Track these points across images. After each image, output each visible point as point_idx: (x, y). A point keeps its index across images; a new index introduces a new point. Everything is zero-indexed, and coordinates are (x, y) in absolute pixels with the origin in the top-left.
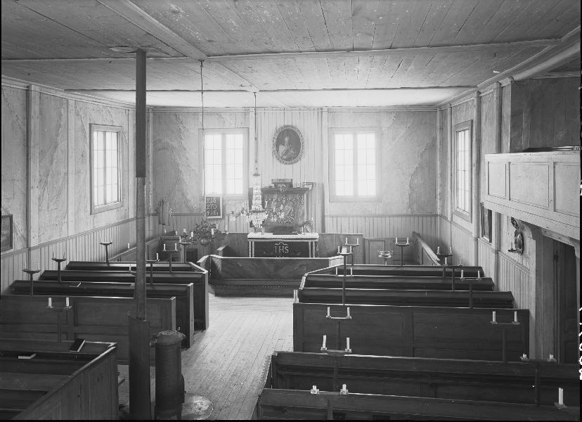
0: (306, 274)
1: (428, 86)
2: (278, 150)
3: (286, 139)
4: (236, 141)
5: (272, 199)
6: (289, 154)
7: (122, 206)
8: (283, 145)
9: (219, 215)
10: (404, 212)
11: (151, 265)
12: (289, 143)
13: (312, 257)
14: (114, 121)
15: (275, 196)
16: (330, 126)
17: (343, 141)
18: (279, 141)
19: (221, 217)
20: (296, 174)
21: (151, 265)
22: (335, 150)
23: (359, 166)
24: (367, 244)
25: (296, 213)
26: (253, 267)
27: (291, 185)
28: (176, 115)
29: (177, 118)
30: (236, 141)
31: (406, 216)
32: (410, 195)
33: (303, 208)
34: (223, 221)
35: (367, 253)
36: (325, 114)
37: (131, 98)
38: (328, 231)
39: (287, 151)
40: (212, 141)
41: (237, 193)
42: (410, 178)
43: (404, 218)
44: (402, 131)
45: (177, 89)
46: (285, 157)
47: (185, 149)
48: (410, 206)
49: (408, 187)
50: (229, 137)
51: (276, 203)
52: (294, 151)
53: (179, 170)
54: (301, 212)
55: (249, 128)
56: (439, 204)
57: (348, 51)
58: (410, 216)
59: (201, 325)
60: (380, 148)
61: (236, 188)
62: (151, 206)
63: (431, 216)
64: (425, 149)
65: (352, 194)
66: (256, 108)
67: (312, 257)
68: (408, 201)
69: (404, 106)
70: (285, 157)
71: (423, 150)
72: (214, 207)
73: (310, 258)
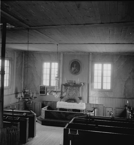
0: (74, 118)
1: (127, 43)
3: (75, 65)
4: (55, 65)
5: (67, 88)
7: (10, 88)
8: (73, 67)
9: (45, 94)
10: (122, 97)
14: (8, 56)
15: (69, 87)
18: (72, 66)
19: (45, 94)
20: (77, 79)
23: (49, 74)
24: (105, 108)
26: (57, 114)
27: (75, 84)
28: (33, 55)
29: (33, 56)
30: (55, 65)
32: (125, 90)
33: (79, 93)
35: (105, 112)
36: (91, 56)
38: (91, 102)
39: (75, 70)
40: (46, 65)
43: (122, 99)
44: (122, 63)
45: (36, 43)
46: (74, 72)
48: (124, 94)
49: (124, 87)
50: (53, 64)
51: (69, 90)
53: (33, 75)
55: (60, 60)
57: (84, 25)
58: (124, 98)
59: (32, 135)
61: (54, 83)
67: (82, 112)
68: (124, 92)
69: (124, 53)
70: (74, 72)
72: (43, 91)
73: (67, 112)
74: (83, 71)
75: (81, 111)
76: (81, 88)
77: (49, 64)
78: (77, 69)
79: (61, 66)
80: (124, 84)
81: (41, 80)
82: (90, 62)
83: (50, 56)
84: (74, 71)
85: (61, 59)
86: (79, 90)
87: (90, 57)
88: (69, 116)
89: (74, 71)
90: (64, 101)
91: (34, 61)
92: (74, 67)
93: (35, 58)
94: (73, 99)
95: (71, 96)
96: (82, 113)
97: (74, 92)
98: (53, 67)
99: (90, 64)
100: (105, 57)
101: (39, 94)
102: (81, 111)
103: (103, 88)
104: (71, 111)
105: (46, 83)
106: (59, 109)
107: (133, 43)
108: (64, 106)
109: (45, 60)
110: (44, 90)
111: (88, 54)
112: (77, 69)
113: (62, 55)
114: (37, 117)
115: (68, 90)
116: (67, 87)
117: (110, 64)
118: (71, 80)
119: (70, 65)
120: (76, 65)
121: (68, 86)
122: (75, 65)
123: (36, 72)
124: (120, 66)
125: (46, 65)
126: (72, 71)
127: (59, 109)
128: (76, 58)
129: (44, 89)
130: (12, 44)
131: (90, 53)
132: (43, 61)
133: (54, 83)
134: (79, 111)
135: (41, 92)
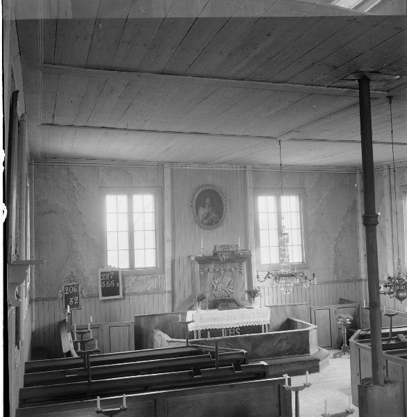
2: (197, 213)
4: (145, 203)
5: (208, 270)
6: (211, 217)
8: (204, 207)
10: (332, 278)
13: (197, 338)
15: (212, 267)
17: (265, 204)
18: (199, 203)
25: (235, 285)
30: (145, 203)
31: (334, 282)
34: (122, 302)
36: (249, 175)
37: (353, 155)
39: (208, 214)
43: (331, 285)
45: (113, 126)
46: (206, 221)
47: (80, 213)
48: (336, 272)
49: (333, 253)
50: (137, 198)
60: (304, 211)
61: (146, 258)
62: (140, 278)
64: (347, 212)
70: (206, 221)
71: (345, 212)
72: (112, 285)
74: (230, 216)
75: (263, 327)
77: (123, 199)
78: (214, 211)
79: (168, 204)
80: (333, 247)
81: (100, 249)
82: (250, 191)
83: (126, 174)
84: (206, 218)
85: (168, 182)
86: (240, 272)
87: (248, 180)
88: (263, 344)
89: (206, 218)
90: (205, 309)
92: (207, 205)
93: (76, 179)
94: (227, 298)
95: (220, 293)
96: (267, 333)
97: (227, 279)
98: (284, 208)
99: (250, 198)
100: (284, 179)
101: (101, 298)
102: (263, 327)
103: (136, 266)
104: (236, 334)
105: (116, 260)
106: (200, 334)
107: (357, 139)
108: (217, 323)
109: (113, 187)
110: (116, 284)
111: (92, 164)
112: (214, 211)
113: (167, 171)
114: (384, 350)
115: (210, 276)
117: (152, 193)
118: (224, 244)
119: (195, 201)
120: (210, 202)
121: (210, 263)
122: (208, 201)
123: (84, 225)
124: (321, 201)
127: (199, 332)
128: (209, 180)
129: (117, 280)
130: (325, 142)
131: (249, 167)
132: (104, 189)
133: (146, 258)
134: (257, 329)
135: (107, 292)
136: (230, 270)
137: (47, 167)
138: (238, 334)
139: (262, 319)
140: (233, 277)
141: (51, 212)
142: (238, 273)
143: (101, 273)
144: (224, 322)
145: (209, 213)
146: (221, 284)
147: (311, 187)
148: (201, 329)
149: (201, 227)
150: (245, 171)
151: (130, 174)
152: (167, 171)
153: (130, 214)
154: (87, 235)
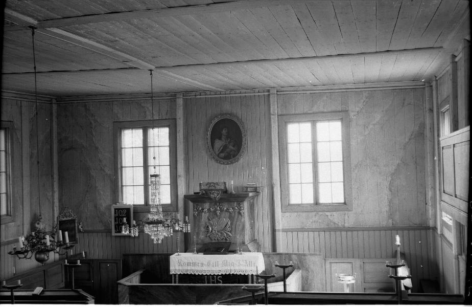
3: (224, 132)
5: (203, 209)
6: (228, 150)
8: (220, 138)
10: (384, 224)
11: (12, 294)
12: (228, 137)
16: (280, 113)
17: (298, 133)
18: (216, 134)
21: (12, 294)
22: (342, 141)
25: (233, 227)
28: (86, 106)
30: (331, 132)
32: (390, 202)
33: (243, 220)
39: (225, 147)
41: (305, 202)
42: (390, 178)
46: (222, 155)
47: (97, 148)
48: (391, 215)
50: (322, 126)
52: (234, 146)
54: (241, 227)
56: (430, 211)
63: (420, 229)
65: (143, 203)
66: (52, 103)
70: (222, 155)
74: (252, 144)
76: (246, 205)
78: (232, 144)
81: (116, 188)
84: (222, 152)
85: (180, 114)
86: (239, 213)
89: (222, 152)
91: (92, 128)
95: (217, 237)
97: (225, 220)
105: (132, 196)
106: (177, 278)
111: (285, 94)
112: (232, 144)
113: (180, 101)
115: (205, 216)
116: (200, 204)
121: (205, 202)
125: (131, 139)
126: (217, 153)
127: (177, 276)
131: (274, 91)
132: (285, 119)
136: (227, 210)
137: (87, 104)
138: (220, 283)
139: (249, 268)
140: (231, 218)
141: (71, 148)
142: (237, 214)
143: (115, 209)
144: (205, 268)
145: (226, 145)
146: (219, 225)
147: (358, 109)
148: (179, 273)
149: (217, 161)
150: (269, 95)
151: (143, 107)
152: (180, 101)
153: (314, 142)
154: (103, 170)
